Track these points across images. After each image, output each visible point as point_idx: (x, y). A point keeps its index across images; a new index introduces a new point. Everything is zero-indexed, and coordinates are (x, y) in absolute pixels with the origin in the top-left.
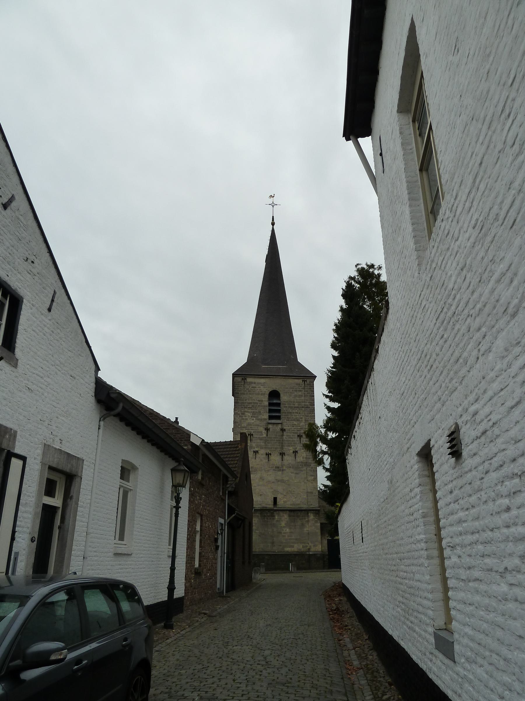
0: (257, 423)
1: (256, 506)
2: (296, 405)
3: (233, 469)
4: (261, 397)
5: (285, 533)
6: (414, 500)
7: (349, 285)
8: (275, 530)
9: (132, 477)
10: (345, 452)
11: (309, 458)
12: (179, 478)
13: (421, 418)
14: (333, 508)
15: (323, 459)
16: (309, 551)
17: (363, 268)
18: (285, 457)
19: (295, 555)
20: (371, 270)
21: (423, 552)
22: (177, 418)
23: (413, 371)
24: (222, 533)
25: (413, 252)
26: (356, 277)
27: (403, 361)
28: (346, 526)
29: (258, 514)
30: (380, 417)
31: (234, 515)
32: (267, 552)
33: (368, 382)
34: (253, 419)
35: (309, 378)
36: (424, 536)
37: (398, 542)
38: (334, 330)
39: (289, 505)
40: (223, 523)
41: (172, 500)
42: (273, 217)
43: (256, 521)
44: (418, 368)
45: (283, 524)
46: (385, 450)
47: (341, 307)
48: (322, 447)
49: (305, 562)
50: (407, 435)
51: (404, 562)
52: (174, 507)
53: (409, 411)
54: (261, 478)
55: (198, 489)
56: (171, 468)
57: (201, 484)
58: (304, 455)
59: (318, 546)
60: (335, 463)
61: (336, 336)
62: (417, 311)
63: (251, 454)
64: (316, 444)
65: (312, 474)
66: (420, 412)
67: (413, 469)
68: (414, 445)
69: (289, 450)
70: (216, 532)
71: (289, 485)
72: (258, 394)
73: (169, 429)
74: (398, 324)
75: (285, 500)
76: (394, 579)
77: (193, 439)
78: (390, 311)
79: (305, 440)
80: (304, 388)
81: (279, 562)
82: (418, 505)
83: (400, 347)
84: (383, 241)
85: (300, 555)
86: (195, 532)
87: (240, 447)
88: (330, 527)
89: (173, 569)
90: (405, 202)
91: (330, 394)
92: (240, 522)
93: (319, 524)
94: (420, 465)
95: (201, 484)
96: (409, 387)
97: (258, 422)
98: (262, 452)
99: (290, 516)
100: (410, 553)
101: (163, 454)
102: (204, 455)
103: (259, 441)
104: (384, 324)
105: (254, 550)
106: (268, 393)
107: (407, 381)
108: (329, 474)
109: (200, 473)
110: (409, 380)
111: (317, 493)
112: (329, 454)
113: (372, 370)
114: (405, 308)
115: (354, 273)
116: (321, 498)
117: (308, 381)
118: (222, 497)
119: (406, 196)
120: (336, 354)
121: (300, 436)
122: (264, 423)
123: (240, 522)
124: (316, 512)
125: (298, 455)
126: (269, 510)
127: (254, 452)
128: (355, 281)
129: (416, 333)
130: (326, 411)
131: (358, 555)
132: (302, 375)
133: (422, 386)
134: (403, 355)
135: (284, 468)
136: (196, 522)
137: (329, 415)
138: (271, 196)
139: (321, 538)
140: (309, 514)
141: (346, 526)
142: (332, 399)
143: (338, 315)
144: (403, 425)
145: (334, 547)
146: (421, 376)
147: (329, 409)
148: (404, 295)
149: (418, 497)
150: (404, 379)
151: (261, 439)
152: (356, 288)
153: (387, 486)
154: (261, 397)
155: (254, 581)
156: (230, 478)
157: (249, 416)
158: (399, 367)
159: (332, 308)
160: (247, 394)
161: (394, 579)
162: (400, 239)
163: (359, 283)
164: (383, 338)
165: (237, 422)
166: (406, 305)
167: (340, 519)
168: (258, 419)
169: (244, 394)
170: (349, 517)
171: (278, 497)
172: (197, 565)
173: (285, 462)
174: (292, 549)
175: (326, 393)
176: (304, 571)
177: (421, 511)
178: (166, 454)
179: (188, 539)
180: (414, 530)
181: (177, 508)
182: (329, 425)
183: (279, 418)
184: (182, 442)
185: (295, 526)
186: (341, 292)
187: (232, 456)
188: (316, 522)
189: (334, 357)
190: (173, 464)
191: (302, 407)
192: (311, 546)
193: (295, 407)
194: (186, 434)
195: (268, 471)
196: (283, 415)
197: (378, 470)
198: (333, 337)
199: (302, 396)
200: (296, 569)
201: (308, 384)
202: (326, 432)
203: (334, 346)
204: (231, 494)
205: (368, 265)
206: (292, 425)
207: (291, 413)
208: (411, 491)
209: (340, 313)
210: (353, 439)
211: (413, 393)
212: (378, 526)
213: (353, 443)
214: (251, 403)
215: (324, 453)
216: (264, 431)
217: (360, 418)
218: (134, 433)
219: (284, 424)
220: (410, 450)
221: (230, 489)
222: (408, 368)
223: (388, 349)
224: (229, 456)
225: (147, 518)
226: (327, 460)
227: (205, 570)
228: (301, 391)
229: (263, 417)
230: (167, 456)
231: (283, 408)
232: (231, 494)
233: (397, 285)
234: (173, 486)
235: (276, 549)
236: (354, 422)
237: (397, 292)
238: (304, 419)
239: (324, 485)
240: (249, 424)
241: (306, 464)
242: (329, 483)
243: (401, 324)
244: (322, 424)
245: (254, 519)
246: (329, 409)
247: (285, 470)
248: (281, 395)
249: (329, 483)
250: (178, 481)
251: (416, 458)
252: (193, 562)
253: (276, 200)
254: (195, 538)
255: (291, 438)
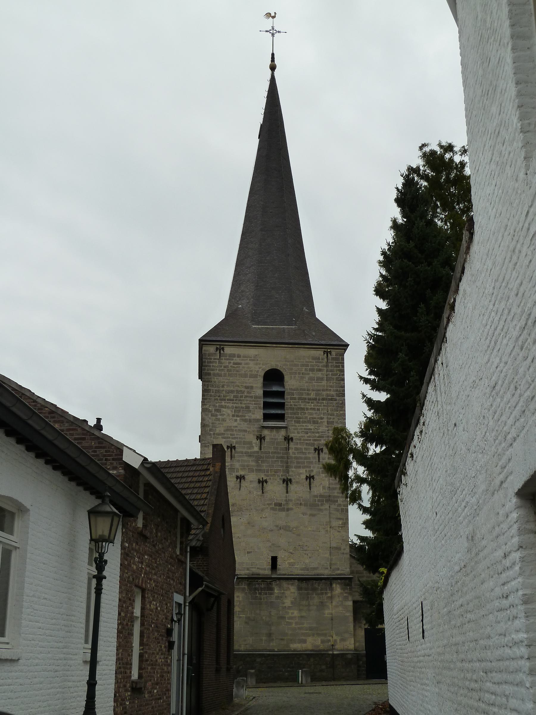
0: (243, 425)
1: (241, 570)
2: (313, 396)
3: (198, 509)
4: (249, 381)
5: (291, 618)
6: (510, 573)
7: (409, 182)
8: (274, 612)
9: (18, 524)
10: (396, 482)
11: (334, 489)
12: (103, 527)
13: (524, 432)
14: (375, 577)
15: (360, 492)
16: (333, 650)
17: (433, 153)
18: (292, 487)
19: (309, 656)
20: (447, 156)
21: (522, 662)
22: (99, 420)
23: (512, 346)
24: (179, 621)
25: (517, 135)
26: (422, 168)
27: (496, 329)
28: (395, 609)
29: (244, 586)
30: (455, 425)
31: (200, 589)
32: (260, 650)
33: (436, 361)
34: (236, 420)
35: (334, 347)
36: (525, 636)
37: (481, 642)
38: (380, 262)
39: (297, 571)
40: (182, 602)
41: (90, 564)
42: (273, 55)
43: (240, 597)
44: (520, 343)
45: (288, 602)
46: (464, 481)
47: (394, 221)
48: (358, 469)
49: (326, 667)
50: (500, 460)
51: (492, 677)
52: (94, 577)
53: (504, 418)
54: (249, 523)
55: (137, 544)
56: (89, 509)
57: (142, 536)
58: (325, 483)
59: (349, 640)
60: (379, 498)
61: (384, 273)
62: (521, 241)
63: (231, 481)
64: (348, 466)
65: (339, 516)
66: (522, 420)
67: (510, 518)
68: (511, 478)
69: (299, 474)
70: (170, 618)
71: (299, 535)
72: (245, 376)
73: (84, 439)
74: (489, 263)
75: (292, 561)
76: (476, 704)
77: (127, 458)
78: (476, 238)
79: (327, 458)
80: (327, 366)
81: (280, 668)
82: (516, 581)
83: (492, 303)
84: (466, 109)
85: (317, 656)
86: (132, 619)
87: (211, 469)
88: (370, 609)
89: (92, 684)
90: (506, 42)
91: (372, 377)
92: (212, 599)
93: (350, 603)
94: (522, 512)
95: (142, 536)
96: (506, 376)
97: (244, 426)
98: (252, 477)
99: (299, 589)
100: (501, 663)
101: (73, 484)
102: (148, 485)
103: (246, 458)
104: (465, 261)
105: (236, 647)
106: (262, 374)
107: (502, 365)
108: (368, 517)
109: (141, 516)
110: (506, 363)
111: (348, 550)
112: (369, 483)
113: (443, 341)
114: (501, 235)
115: (418, 162)
116: (354, 557)
117: (334, 353)
118: (180, 557)
119: (506, 30)
120: (383, 305)
121: (318, 450)
122: (254, 428)
123: (212, 599)
124: (346, 582)
125: (315, 483)
126: (264, 579)
127: (237, 477)
128: (419, 175)
129: (518, 281)
130: (365, 407)
131: (416, 659)
132: (323, 342)
133: (527, 376)
134: (497, 318)
135: (290, 506)
136: (134, 601)
137: (370, 414)
138: (268, 15)
139: (354, 626)
140: (334, 585)
141: (395, 609)
142: (375, 386)
143: (388, 236)
144: (495, 440)
145: (376, 642)
146: (525, 358)
147: (370, 402)
148: (499, 211)
149: (517, 568)
150: (497, 360)
151: (250, 455)
152: (421, 188)
153: (466, 545)
154: (249, 381)
155: (236, 700)
156: (194, 523)
157: (229, 415)
158: (489, 338)
159: (377, 224)
160: (225, 375)
161: (476, 704)
162: (494, 110)
163: (425, 177)
164: (463, 285)
165: (208, 426)
166: (502, 230)
167: (386, 595)
168: (245, 420)
169: (220, 375)
170: (405, 592)
171: (279, 556)
172: (135, 675)
173: (292, 496)
174: (304, 645)
175: (365, 374)
176: (324, 683)
177: (520, 593)
178: (78, 484)
179: (119, 632)
180: (510, 623)
181: (100, 578)
182: (369, 432)
183: (281, 417)
184: (108, 463)
185: (309, 605)
186: (394, 194)
187: (198, 485)
188: (346, 599)
189: (380, 311)
190: (92, 502)
191: (323, 399)
192: (335, 641)
193: (309, 399)
194: (116, 449)
195: (262, 510)
196: (288, 413)
197: (450, 515)
198: (379, 275)
199: (322, 379)
200: (309, 680)
201: (333, 359)
202: (364, 445)
203: (379, 291)
204: (195, 552)
205: (441, 147)
206: (306, 430)
207: (303, 409)
208: (505, 556)
209: (392, 233)
210: (409, 460)
211: (512, 387)
212: (450, 612)
213: (410, 466)
214: (232, 392)
215: (361, 480)
216: (256, 442)
217: (421, 423)
218: (22, 448)
219: (291, 428)
220: (504, 485)
221: (193, 544)
222: (505, 341)
223: (470, 306)
224: (192, 485)
225: (46, 596)
226: (366, 493)
227: (149, 684)
228: (320, 370)
229: (253, 417)
230: (81, 488)
231: (288, 401)
232: (195, 552)
233: (488, 192)
234: (92, 540)
235: (275, 646)
236: (412, 428)
237: (488, 204)
238: (325, 420)
239: (360, 537)
240: (229, 429)
241: (330, 499)
242: (368, 534)
243: (494, 263)
244: (358, 430)
245: (236, 594)
246: (370, 402)
247: (292, 509)
248: (286, 378)
249: (368, 534)
250: (100, 533)
251: (514, 500)
252: (128, 671)
253: (278, 24)
254: (132, 630)
255: (303, 453)
